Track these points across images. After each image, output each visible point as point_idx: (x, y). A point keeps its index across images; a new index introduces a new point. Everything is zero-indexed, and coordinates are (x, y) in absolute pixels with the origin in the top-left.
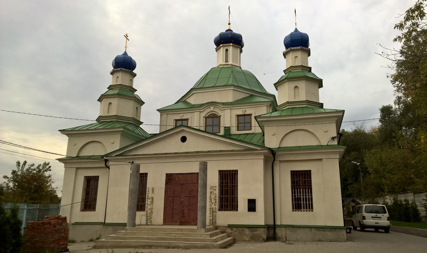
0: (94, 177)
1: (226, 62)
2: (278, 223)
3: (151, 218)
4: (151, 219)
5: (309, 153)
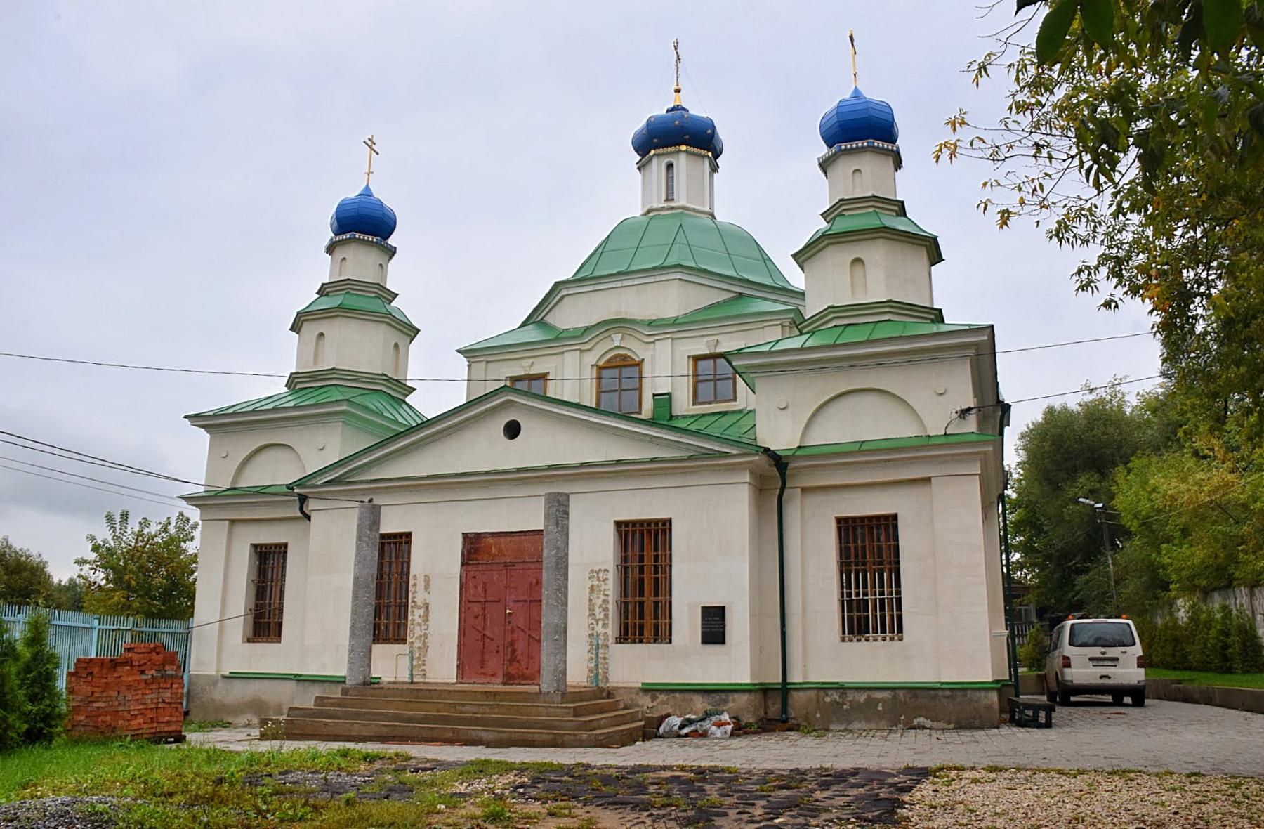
0: (276, 546)
1: (667, 200)
3: (424, 665)
4: (423, 667)
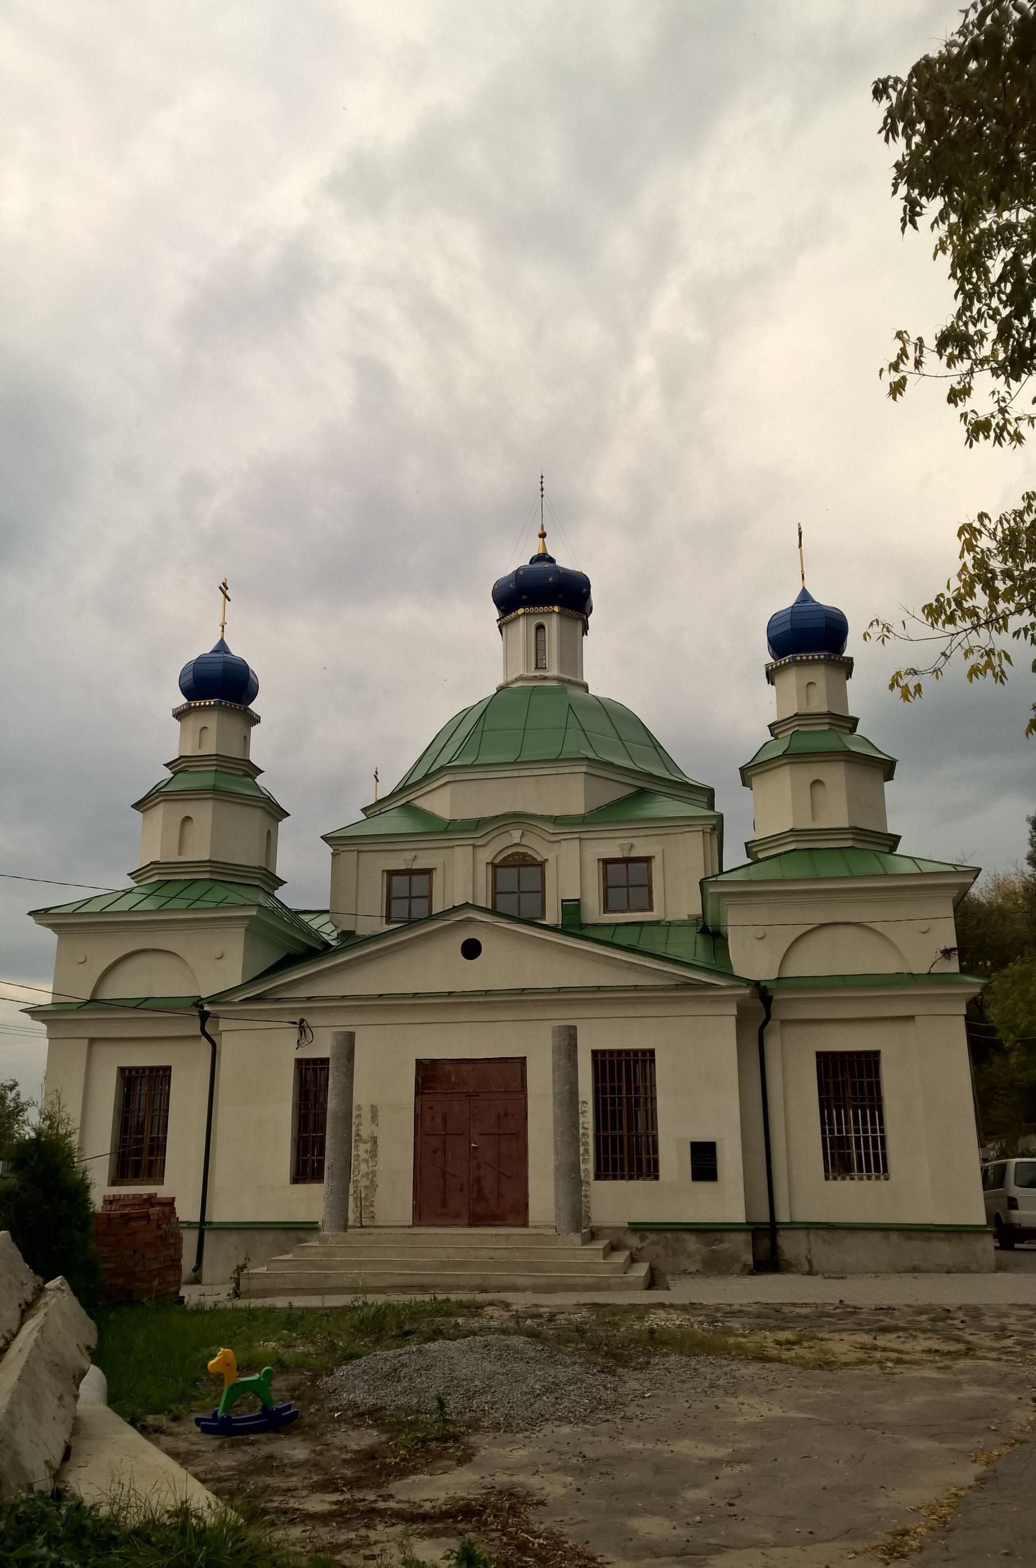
2: (783, 1216)
3: (372, 1206)
4: (371, 1209)
5: (874, 997)
